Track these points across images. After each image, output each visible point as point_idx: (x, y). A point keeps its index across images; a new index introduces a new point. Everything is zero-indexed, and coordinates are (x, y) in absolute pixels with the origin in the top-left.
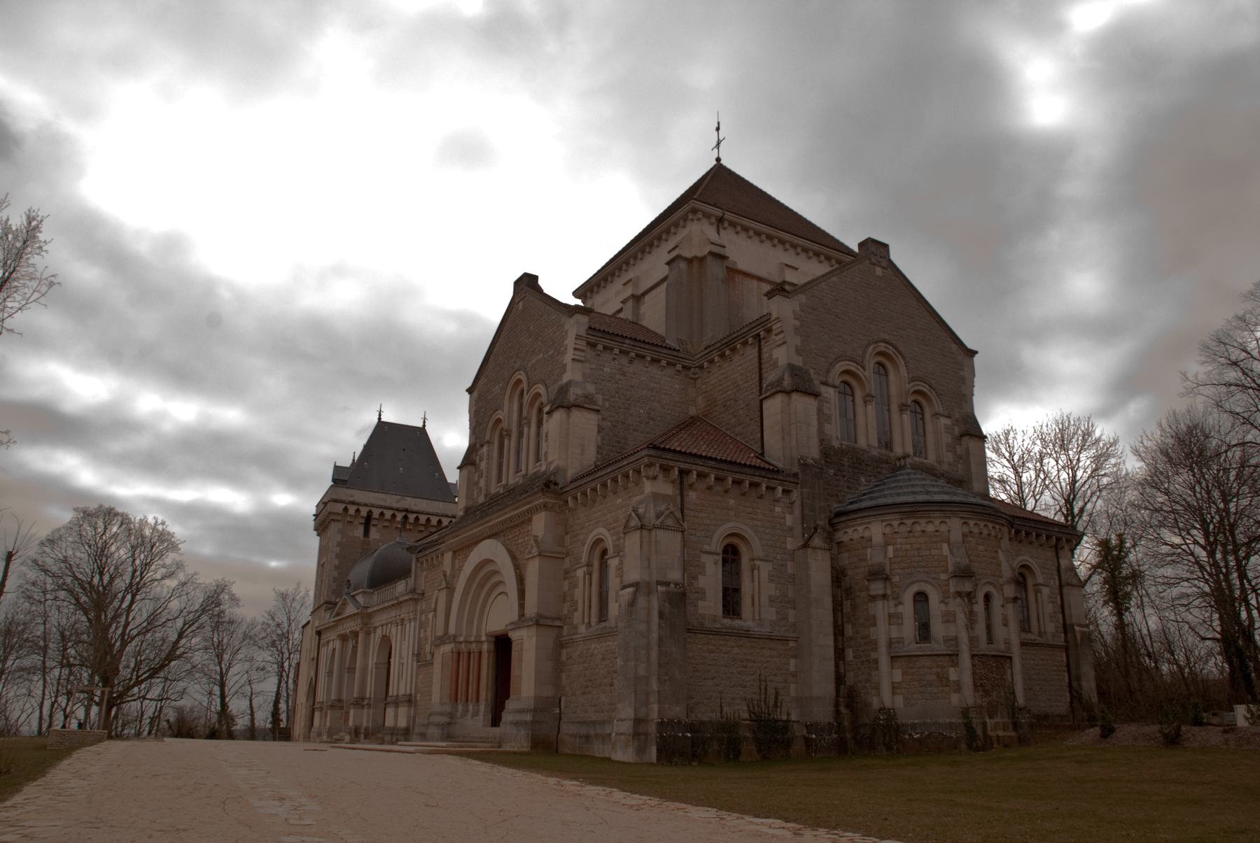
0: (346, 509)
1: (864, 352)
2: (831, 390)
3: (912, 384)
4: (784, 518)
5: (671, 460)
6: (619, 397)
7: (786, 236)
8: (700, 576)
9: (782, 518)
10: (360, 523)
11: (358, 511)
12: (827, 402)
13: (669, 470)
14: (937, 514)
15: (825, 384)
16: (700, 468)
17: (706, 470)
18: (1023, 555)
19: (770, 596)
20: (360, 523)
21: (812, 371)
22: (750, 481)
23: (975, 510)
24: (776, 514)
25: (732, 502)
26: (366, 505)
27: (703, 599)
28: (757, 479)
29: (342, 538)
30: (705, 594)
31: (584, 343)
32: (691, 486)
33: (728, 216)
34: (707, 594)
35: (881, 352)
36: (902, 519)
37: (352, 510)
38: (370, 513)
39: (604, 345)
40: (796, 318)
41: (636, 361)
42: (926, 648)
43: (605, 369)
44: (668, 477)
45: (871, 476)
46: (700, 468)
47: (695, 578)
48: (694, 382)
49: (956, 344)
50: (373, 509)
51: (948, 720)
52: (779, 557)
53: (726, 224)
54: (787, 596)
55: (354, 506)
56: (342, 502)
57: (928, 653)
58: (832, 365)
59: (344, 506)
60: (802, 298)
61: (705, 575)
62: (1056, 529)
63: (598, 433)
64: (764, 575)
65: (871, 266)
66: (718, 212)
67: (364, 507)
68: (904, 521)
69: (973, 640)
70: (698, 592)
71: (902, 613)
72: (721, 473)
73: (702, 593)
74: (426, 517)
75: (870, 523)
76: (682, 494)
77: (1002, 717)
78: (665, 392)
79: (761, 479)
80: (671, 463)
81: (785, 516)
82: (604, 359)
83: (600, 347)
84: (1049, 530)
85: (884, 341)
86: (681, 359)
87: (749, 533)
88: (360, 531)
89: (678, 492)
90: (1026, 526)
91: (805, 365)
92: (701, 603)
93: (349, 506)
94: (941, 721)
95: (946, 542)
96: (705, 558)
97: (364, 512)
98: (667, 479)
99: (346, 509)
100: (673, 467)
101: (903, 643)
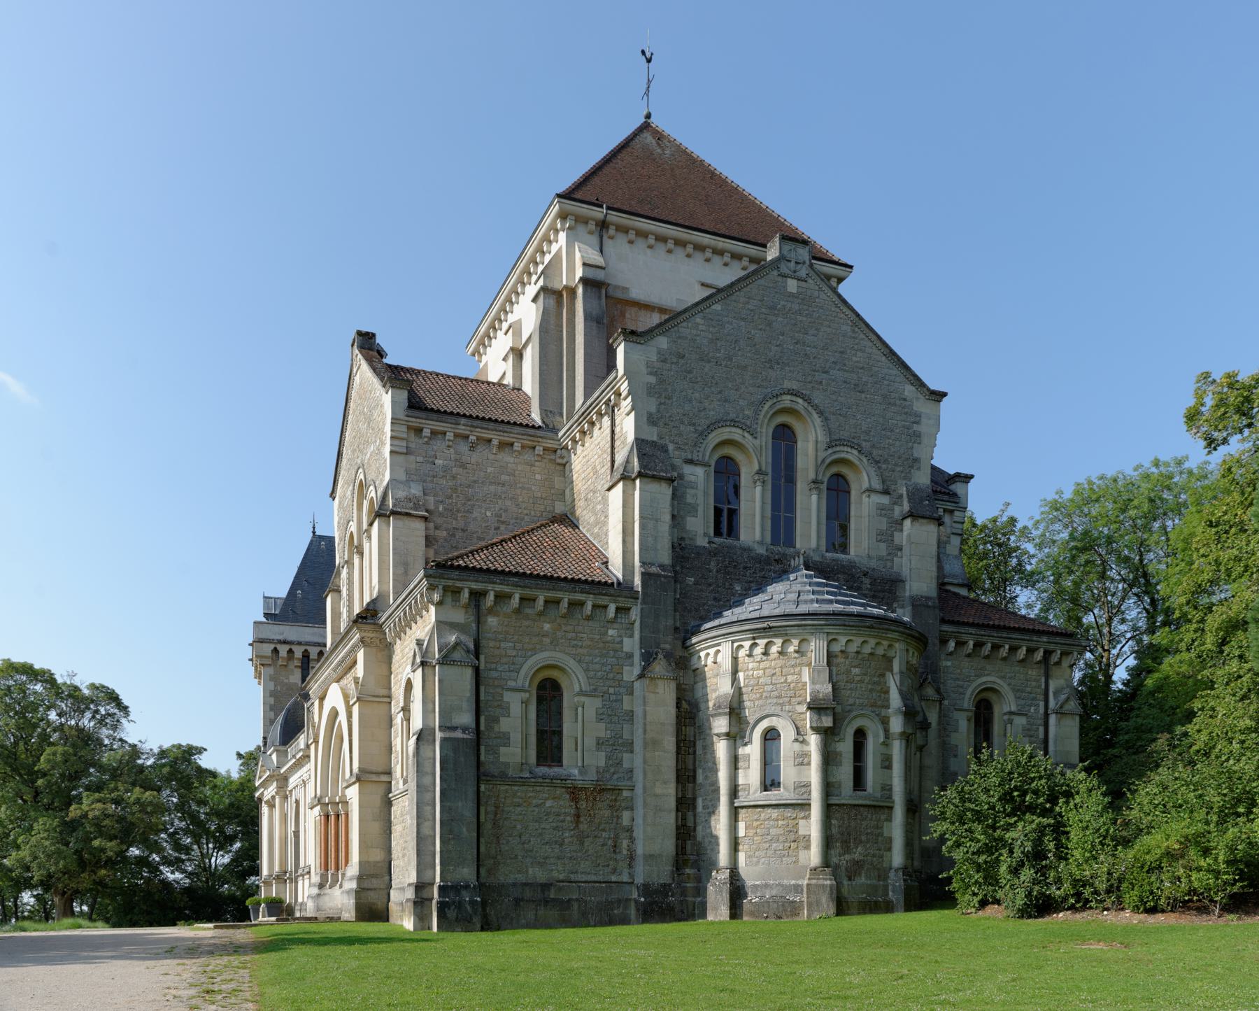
0: (276, 651)
1: (757, 413)
2: (700, 471)
3: (830, 451)
4: (621, 642)
5: (457, 580)
6: (458, 497)
7: (705, 239)
8: (502, 719)
9: (618, 643)
10: (296, 667)
11: (290, 651)
12: (692, 488)
13: (459, 592)
14: (795, 630)
15: (690, 462)
16: (498, 588)
17: (507, 589)
18: (988, 675)
19: (598, 739)
20: (296, 667)
21: (671, 447)
22: (569, 599)
23: (847, 623)
24: (609, 638)
25: (547, 626)
26: (300, 643)
27: (507, 745)
28: (579, 597)
29: (275, 686)
30: (509, 739)
31: (404, 429)
32: (491, 611)
33: (614, 217)
34: (511, 739)
35: (785, 408)
36: (754, 638)
37: (283, 650)
38: (306, 654)
39: (431, 429)
40: (650, 373)
41: (479, 447)
42: (773, 796)
43: (436, 461)
44: (459, 601)
45: (750, 582)
46: (498, 588)
47: (497, 720)
48: (562, 468)
49: (912, 384)
50: (310, 649)
51: (793, 882)
52: (611, 690)
53: (612, 231)
54: (621, 737)
55: (316, 648)
56: (270, 641)
57: (774, 802)
58: (703, 434)
59: (272, 646)
60: (662, 342)
61: (509, 716)
62: (1045, 639)
63: (427, 546)
64: (591, 713)
65: (780, 279)
66: (599, 213)
67: (298, 646)
68: (756, 641)
69: (828, 788)
70: (499, 738)
71: (749, 755)
72: (528, 592)
73: (505, 739)
74: (302, 648)
75: (719, 645)
76: (478, 622)
77: (868, 877)
78: (521, 485)
79: (584, 595)
80: (459, 584)
81: (622, 641)
82: (435, 447)
83: (427, 432)
84: (1032, 641)
85: (791, 392)
86: (540, 440)
87: (570, 664)
88: (296, 677)
89: (472, 618)
90: (993, 636)
91: (661, 438)
92: (503, 750)
93: (279, 647)
94: (785, 882)
95: (806, 665)
96: (507, 696)
97: (298, 651)
98: (458, 604)
99: (276, 651)
100: (462, 588)
101: (749, 791)
